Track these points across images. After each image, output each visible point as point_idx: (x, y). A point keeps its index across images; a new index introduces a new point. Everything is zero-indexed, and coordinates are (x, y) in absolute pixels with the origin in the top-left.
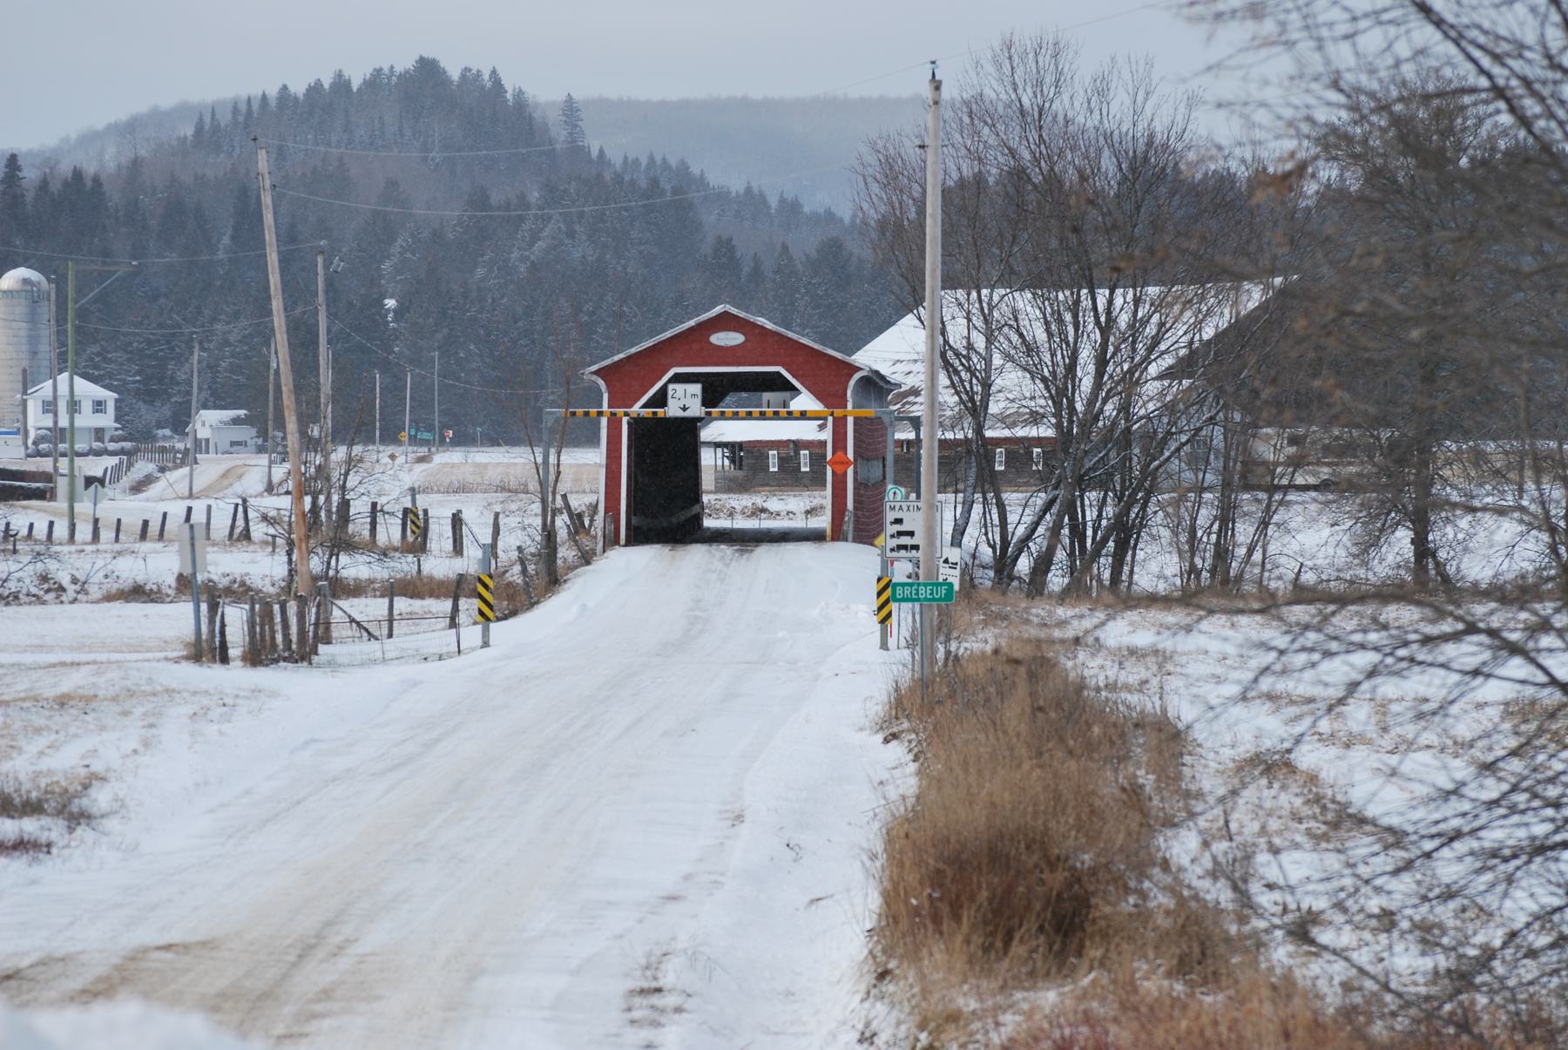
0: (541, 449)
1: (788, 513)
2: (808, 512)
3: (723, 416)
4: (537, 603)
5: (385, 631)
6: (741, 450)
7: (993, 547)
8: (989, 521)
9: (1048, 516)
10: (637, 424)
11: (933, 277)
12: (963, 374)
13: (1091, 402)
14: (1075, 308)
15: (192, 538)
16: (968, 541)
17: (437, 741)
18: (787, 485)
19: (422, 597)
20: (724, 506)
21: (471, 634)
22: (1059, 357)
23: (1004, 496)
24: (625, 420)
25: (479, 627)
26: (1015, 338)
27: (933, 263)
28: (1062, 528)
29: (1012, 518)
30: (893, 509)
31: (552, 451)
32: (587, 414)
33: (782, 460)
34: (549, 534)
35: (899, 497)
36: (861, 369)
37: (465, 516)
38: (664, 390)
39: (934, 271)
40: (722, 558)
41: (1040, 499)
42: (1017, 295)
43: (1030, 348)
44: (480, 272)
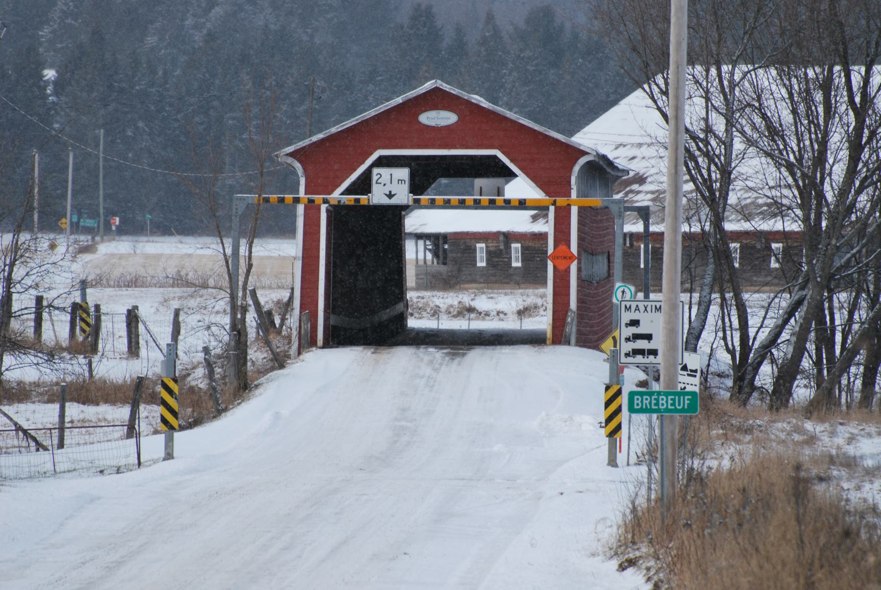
0: (230, 240)
1: (498, 313)
3: (432, 204)
4: (226, 410)
5: (56, 441)
6: (445, 243)
7: (732, 352)
8: (728, 324)
9: (792, 321)
10: (337, 213)
11: (678, 50)
12: (700, 160)
13: (843, 193)
14: (827, 86)
16: (704, 345)
17: (119, 564)
18: (496, 282)
19: (97, 404)
20: (427, 304)
21: (153, 445)
22: (807, 143)
23: (746, 296)
24: (324, 207)
25: (161, 438)
26: (758, 120)
27: (678, 35)
28: (810, 332)
29: (753, 322)
30: (628, 309)
31: (243, 243)
32: (282, 200)
33: (491, 255)
34: (238, 330)
35: (628, 296)
36: (587, 153)
37: (142, 312)
38: (367, 175)
39: (679, 44)
40: (431, 362)
41: (784, 301)
42: (761, 72)
43: (774, 131)
44: (151, 40)
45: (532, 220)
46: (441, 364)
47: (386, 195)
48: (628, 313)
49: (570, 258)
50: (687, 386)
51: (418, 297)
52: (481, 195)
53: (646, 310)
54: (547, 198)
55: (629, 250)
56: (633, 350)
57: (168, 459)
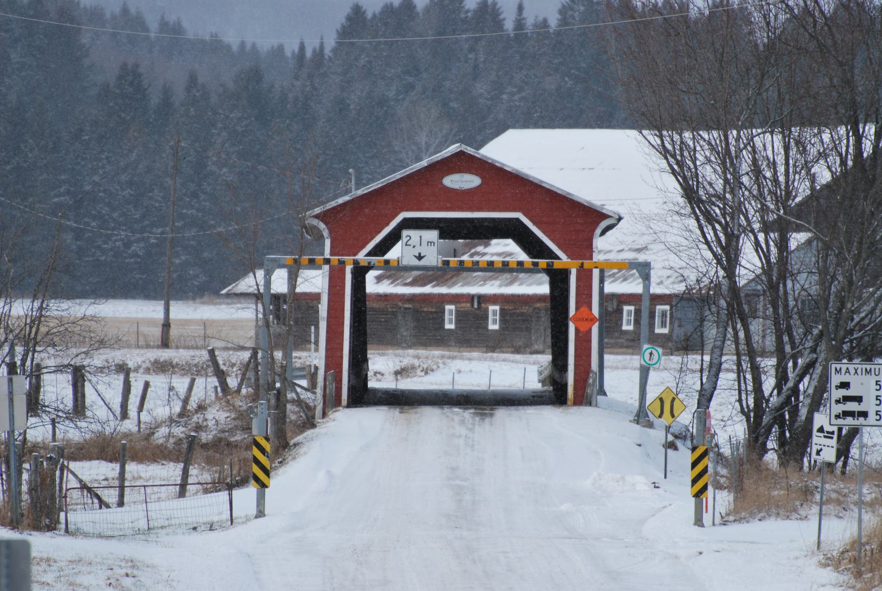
2: (397, 373)
8: (743, 387)
15: (11, 393)
33: (461, 317)
40: (462, 422)
45: (375, 281)
46: (473, 424)
47: (415, 256)
48: (838, 375)
49: (591, 320)
50: (823, 448)
53: (856, 372)
54: (569, 260)
55: (477, 312)
56: (844, 412)
57: (260, 517)
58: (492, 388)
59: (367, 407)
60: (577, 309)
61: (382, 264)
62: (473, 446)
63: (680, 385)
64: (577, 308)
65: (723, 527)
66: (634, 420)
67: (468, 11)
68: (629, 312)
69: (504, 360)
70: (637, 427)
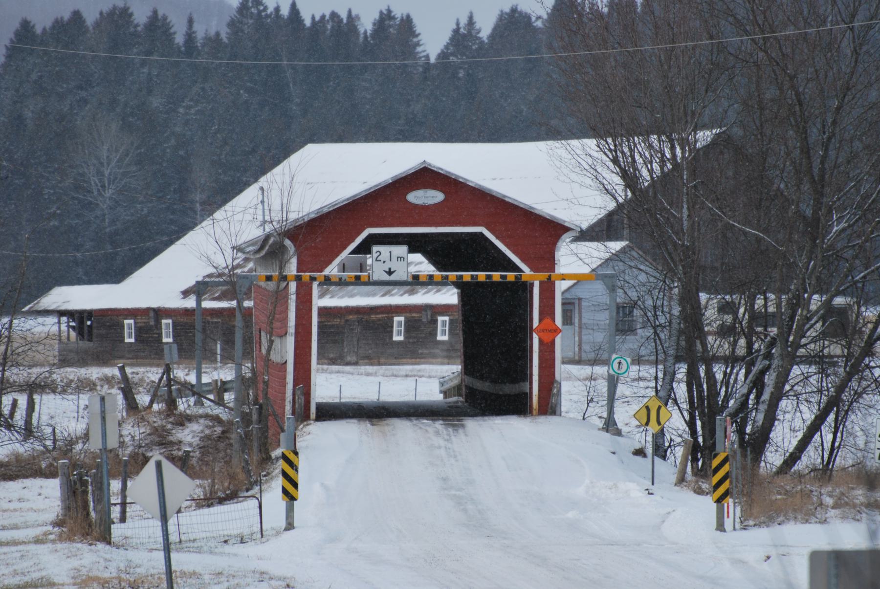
33: (141, 332)
40: (437, 433)
45: (182, 296)
49: (555, 331)
51: (133, 373)
52: (361, 272)
54: (532, 273)
57: (289, 530)
58: (343, 400)
59: (335, 420)
60: (540, 320)
61: (353, 280)
62: (455, 457)
63: (591, 393)
64: (541, 320)
65: (744, 532)
66: (603, 428)
67: (137, 25)
68: (444, 323)
69: (338, 372)
70: (608, 435)
